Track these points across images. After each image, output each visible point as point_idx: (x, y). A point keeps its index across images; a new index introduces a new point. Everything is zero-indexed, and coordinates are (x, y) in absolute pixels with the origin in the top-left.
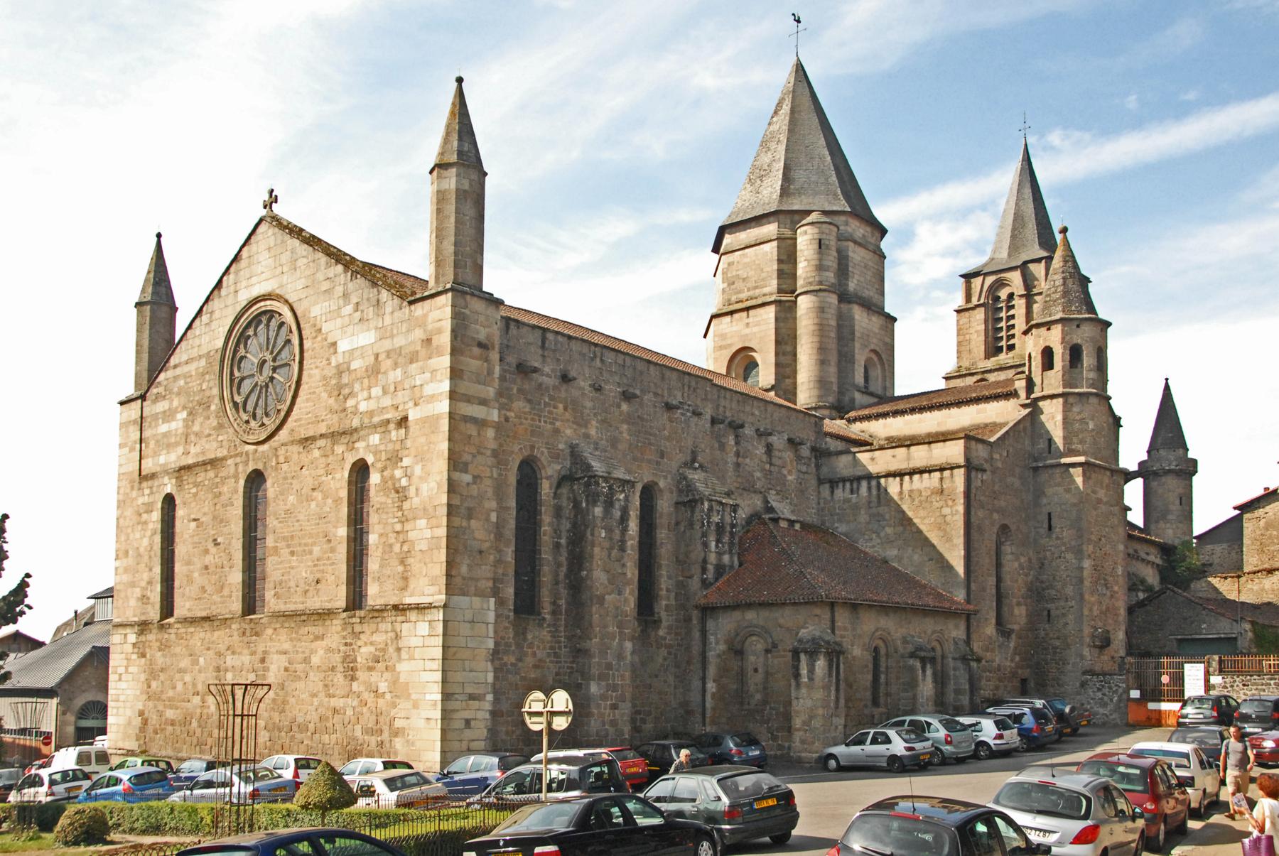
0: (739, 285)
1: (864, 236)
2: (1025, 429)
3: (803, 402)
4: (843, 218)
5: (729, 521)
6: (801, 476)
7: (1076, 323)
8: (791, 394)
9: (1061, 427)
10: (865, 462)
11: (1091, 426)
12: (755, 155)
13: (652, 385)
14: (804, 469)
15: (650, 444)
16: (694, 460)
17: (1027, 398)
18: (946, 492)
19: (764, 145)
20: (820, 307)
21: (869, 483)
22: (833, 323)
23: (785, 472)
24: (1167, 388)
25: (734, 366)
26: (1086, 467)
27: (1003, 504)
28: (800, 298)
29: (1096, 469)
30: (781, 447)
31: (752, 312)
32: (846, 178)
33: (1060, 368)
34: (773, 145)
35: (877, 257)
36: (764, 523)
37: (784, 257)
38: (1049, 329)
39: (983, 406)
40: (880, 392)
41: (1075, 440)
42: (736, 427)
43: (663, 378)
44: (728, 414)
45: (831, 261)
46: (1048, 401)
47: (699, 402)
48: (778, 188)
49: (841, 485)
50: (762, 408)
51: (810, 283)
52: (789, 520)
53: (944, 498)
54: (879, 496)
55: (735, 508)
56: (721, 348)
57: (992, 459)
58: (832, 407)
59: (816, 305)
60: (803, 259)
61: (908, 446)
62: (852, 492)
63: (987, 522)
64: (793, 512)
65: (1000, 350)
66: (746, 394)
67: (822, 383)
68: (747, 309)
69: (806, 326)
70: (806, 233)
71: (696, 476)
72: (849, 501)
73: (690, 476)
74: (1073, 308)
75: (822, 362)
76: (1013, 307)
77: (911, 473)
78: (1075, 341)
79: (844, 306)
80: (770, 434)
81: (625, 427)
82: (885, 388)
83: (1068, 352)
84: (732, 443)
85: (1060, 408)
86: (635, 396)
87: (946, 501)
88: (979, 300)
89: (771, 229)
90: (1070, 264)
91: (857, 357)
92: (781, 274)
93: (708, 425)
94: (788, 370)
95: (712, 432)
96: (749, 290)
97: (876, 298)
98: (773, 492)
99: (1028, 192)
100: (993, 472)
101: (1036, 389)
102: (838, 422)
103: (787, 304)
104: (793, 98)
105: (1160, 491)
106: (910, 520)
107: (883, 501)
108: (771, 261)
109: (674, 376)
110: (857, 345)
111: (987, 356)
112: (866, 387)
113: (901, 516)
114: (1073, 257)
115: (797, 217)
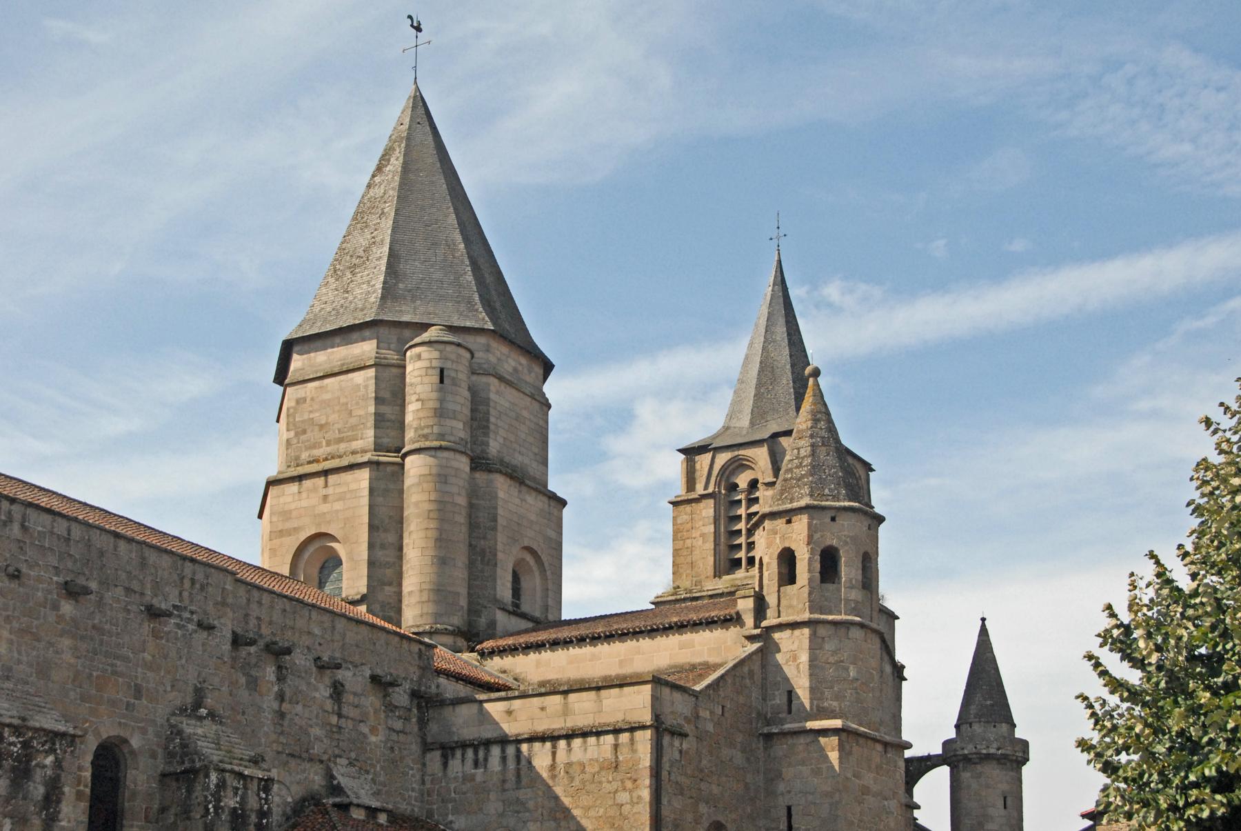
0: (313, 435)
1: (515, 370)
2: (751, 673)
3: (411, 623)
4: (482, 340)
5: (256, 806)
6: (394, 737)
7: (832, 513)
8: (394, 611)
9: (807, 673)
10: (496, 717)
11: (852, 673)
12: (344, 232)
13: (123, 576)
14: (398, 725)
15: (114, 673)
16: (198, 705)
17: (756, 627)
18: (622, 768)
19: (360, 218)
20: (439, 475)
21: (503, 751)
22: (462, 501)
23: (364, 729)
24: (984, 632)
25: (302, 565)
26: (844, 735)
27: (715, 790)
28: (408, 460)
29: (862, 741)
30: (359, 689)
31: (332, 479)
32: (489, 279)
33: (806, 582)
34: (373, 220)
35: (536, 405)
36: (325, 812)
37: (386, 395)
38: (789, 522)
39: (688, 637)
40: (537, 614)
41: (827, 693)
42: (277, 652)
43: (143, 564)
44: (265, 631)
45: (460, 402)
46: (788, 633)
47: (210, 608)
48: (379, 286)
49: (458, 753)
50: (327, 625)
51: (426, 437)
52: (368, 808)
53: (620, 776)
54: (518, 771)
55: (266, 785)
56: (281, 533)
57: (698, 717)
58: (457, 633)
59: (434, 471)
60: (414, 398)
61: (565, 693)
62: (476, 764)
63: (689, 817)
64: (377, 794)
65: (736, 564)
66: (298, 600)
67: (440, 593)
68: (326, 473)
69: (417, 504)
70: (419, 357)
71: (199, 732)
72: (472, 778)
73: (189, 730)
74: (827, 491)
75: (442, 562)
76: (756, 500)
77: (569, 736)
78: (828, 543)
79: (481, 477)
80: (338, 667)
81: (66, 642)
82: (546, 608)
83: (818, 558)
84: (273, 678)
85: (806, 643)
86: (86, 591)
87: (622, 781)
88: (706, 488)
89: (366, 349)
90: (822, 424)
91: (500, 555)
92: (379, 420)
93: (227, 647)
94: (389, 572)
95: (234, 659)
96: (328, 444)
97: (533, 468)
98: (344, 761)
99: (781, 330)
100: (699, 739)
101: (769, 613)
102: (466, 656)
103: (389, 469)
104: (407, 146)
105: (974, 785)
106: (566, 812)
107: (525, 781)
108: (365, 398)
109: (166, 561)
110: (501, 538)
111: (718, 574)
112: (517, 606)
113: (552, 804)
114: (828, 414)
115: (407, 333)
